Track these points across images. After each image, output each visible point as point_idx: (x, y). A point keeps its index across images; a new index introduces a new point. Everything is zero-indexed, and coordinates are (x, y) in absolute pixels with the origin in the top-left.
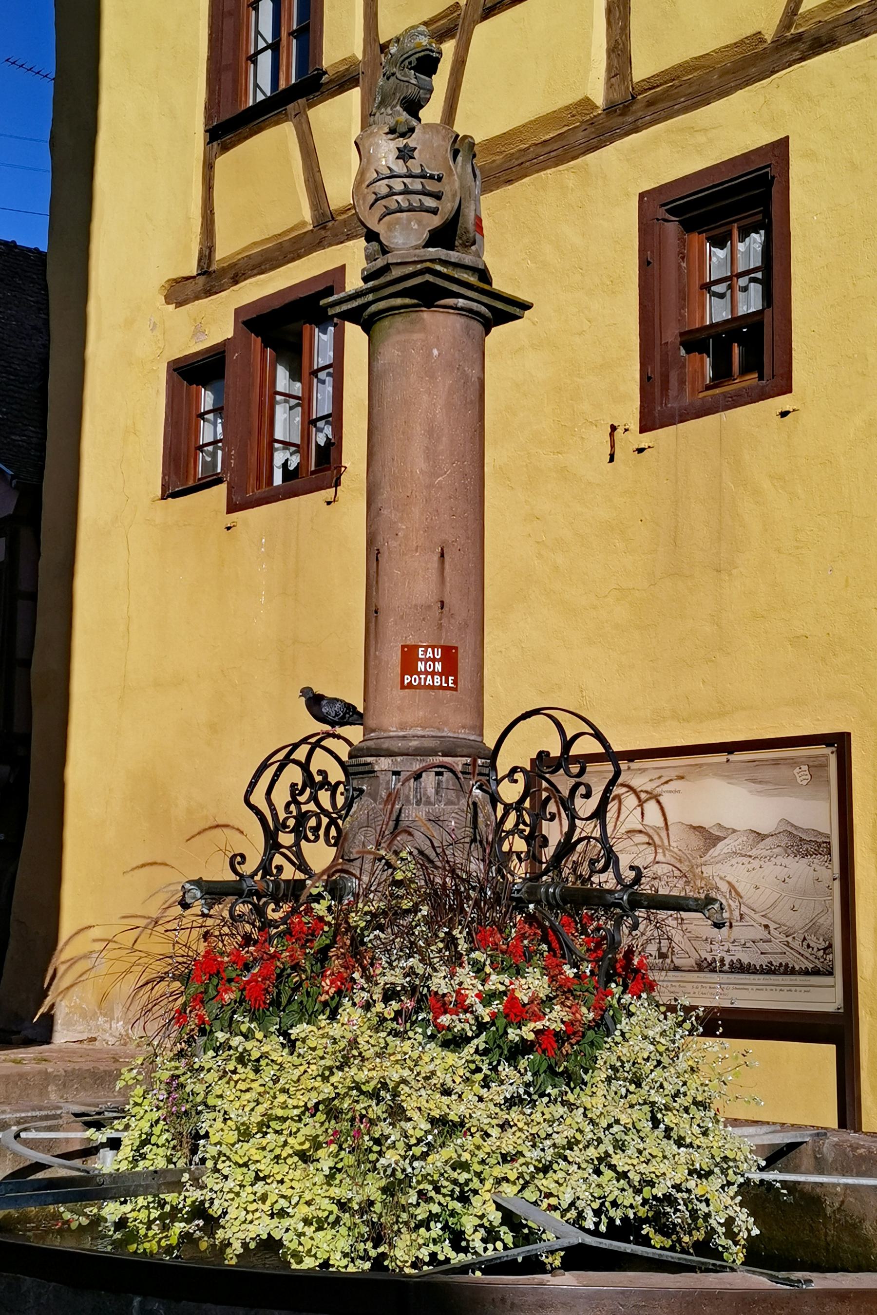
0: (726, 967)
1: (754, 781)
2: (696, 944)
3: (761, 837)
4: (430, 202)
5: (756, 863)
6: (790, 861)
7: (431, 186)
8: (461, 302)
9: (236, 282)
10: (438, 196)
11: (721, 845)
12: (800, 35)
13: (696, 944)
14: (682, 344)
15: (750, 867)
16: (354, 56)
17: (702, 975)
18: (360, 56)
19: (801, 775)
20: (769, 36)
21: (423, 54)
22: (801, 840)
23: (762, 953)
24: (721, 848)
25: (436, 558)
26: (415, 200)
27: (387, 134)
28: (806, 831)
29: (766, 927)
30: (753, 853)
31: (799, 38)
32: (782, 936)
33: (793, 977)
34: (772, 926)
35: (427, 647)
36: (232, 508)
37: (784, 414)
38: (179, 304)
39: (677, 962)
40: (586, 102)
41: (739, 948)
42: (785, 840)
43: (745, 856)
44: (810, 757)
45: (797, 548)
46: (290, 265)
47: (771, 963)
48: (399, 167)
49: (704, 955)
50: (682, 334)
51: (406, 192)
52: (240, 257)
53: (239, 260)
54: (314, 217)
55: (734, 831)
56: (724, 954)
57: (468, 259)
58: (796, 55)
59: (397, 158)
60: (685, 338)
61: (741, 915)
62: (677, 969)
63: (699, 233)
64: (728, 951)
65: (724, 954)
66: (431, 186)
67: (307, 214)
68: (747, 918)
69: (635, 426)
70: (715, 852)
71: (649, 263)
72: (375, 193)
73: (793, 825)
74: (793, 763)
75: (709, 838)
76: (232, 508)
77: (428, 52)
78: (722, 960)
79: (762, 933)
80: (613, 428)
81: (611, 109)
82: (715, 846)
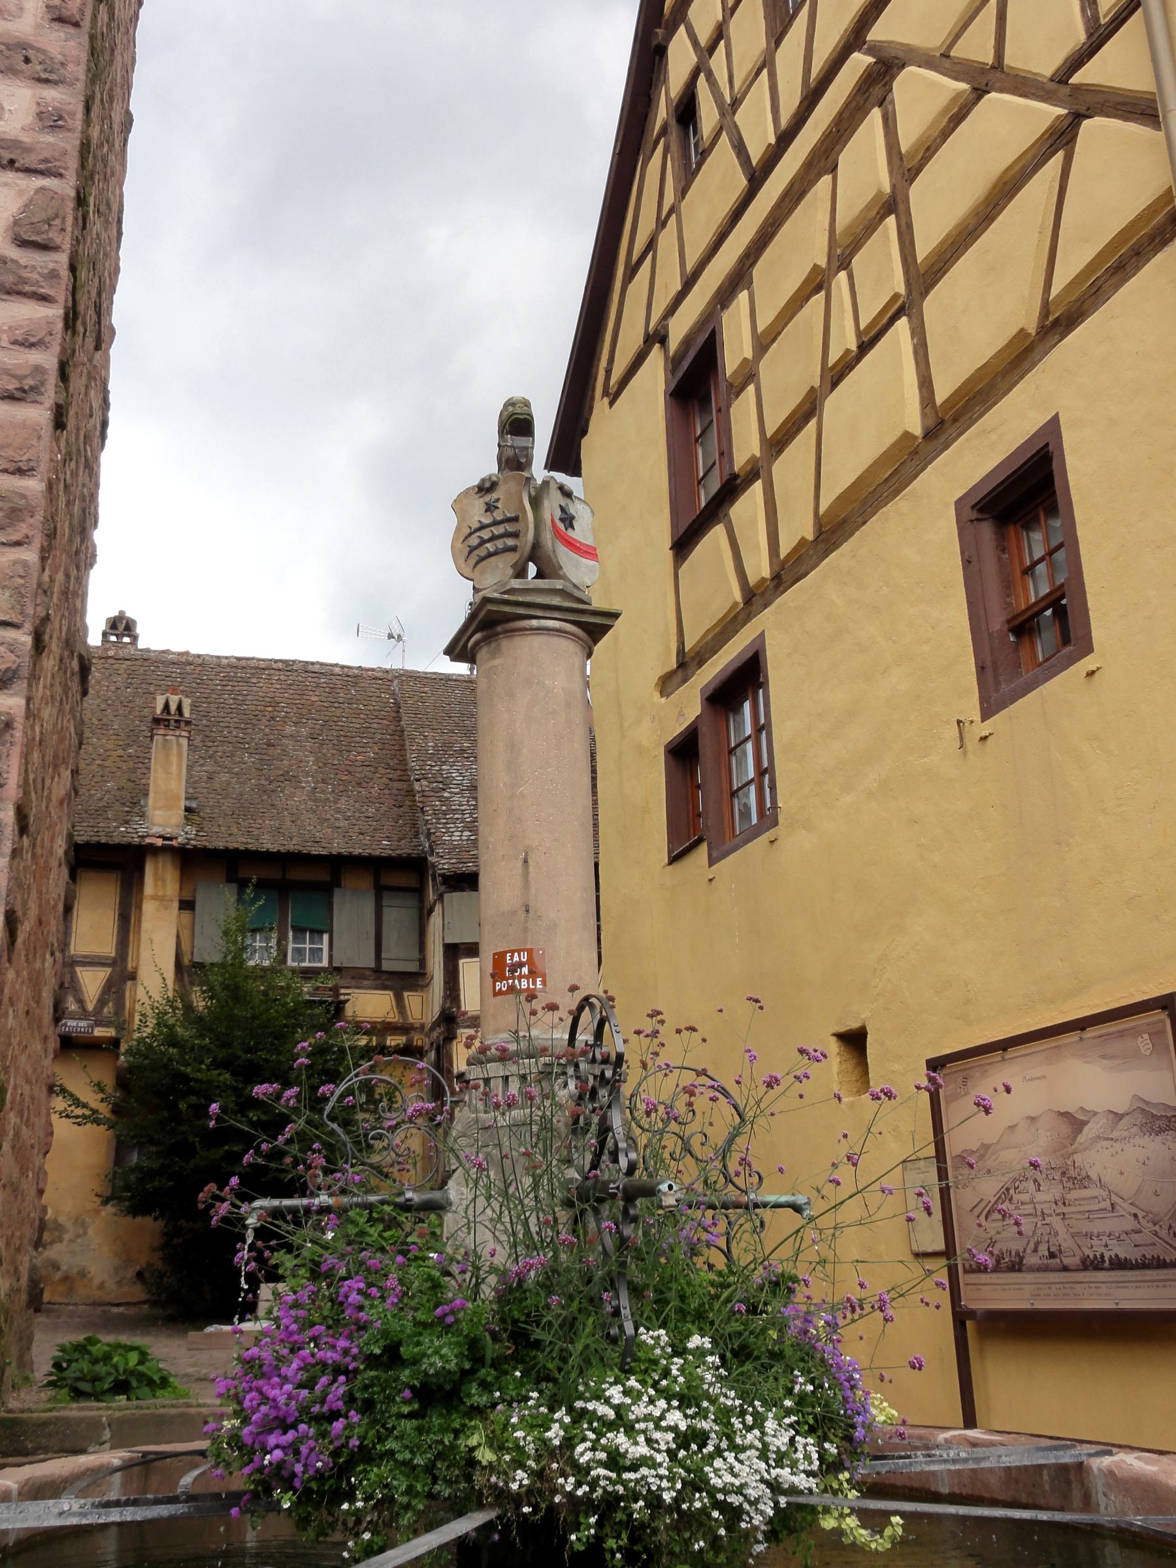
0: (1107, 1264)
1: (1104, 1057)
2: (1079, 1240)
3: (1119, 1117)
4: (510, 542)
5: (1118, 1146)
6: (1146, 1140)
7: (510, 528)
8: (534, 623)
9: (700, 667)
10: (515, 535)
11: (1086, 1129)
12: (1057, 319)
13: (1079, 1240)
14: (1010, 630)
15: (1113, 1150)
16: (754, 456)
17: (1087, 1274)
18: (758, 454)
19: (1144, 1044)
20: (1032, 330)
22: (1153, 1116)
23: (1136, 1246)
24: (1088, 1133)
25: (520, 864)
26: (500, 544)
28: (1156, 1105)
29: (1135, 1216)
30: (1114, 1135)
31: (1056, 322)
32: (1150, 1225)
33: (1166, 1271)
34: (1140, 1214)
35: (513, 952)
36: (712, 862)
37: (1091, 674)
38: (668, 696)
39: (1066, 1261)
40: (907, 436)
41: (1115, 1242)
42: (1139, 1118)
43: (1107, 1139)
44: (1149, 1024)
45: (1119, 806)
47: (1144, 1256)
48: (486, 520)
49: (1087, 1252)
50: (1008, 621)
51: (493, 538)
54: (743, 597)
55: (1095, 1113)
56: (1103, 1250)
57: (558, 584)
58: (1057, 337)
60: (1012, 624)
61: (1112, 1205)
62: (1065, 1269)
63: (1015, 523)
64: (1106, 1246)
65: (1103, 1250)
66: (510, 528)
67: (738, 596)
68: (1118, 1207)
69: (976, 716)
70: (1081, 1138)
71: (969, 562)
73: (1144, 1101)
74: (1135, 1033)
75: (1074, 1123)
76: (712, 862)
78: (1102, 1256)
79: (1130, 1224)
80: (959, 722)
81: (929, 435)
82: (1081, 1131)
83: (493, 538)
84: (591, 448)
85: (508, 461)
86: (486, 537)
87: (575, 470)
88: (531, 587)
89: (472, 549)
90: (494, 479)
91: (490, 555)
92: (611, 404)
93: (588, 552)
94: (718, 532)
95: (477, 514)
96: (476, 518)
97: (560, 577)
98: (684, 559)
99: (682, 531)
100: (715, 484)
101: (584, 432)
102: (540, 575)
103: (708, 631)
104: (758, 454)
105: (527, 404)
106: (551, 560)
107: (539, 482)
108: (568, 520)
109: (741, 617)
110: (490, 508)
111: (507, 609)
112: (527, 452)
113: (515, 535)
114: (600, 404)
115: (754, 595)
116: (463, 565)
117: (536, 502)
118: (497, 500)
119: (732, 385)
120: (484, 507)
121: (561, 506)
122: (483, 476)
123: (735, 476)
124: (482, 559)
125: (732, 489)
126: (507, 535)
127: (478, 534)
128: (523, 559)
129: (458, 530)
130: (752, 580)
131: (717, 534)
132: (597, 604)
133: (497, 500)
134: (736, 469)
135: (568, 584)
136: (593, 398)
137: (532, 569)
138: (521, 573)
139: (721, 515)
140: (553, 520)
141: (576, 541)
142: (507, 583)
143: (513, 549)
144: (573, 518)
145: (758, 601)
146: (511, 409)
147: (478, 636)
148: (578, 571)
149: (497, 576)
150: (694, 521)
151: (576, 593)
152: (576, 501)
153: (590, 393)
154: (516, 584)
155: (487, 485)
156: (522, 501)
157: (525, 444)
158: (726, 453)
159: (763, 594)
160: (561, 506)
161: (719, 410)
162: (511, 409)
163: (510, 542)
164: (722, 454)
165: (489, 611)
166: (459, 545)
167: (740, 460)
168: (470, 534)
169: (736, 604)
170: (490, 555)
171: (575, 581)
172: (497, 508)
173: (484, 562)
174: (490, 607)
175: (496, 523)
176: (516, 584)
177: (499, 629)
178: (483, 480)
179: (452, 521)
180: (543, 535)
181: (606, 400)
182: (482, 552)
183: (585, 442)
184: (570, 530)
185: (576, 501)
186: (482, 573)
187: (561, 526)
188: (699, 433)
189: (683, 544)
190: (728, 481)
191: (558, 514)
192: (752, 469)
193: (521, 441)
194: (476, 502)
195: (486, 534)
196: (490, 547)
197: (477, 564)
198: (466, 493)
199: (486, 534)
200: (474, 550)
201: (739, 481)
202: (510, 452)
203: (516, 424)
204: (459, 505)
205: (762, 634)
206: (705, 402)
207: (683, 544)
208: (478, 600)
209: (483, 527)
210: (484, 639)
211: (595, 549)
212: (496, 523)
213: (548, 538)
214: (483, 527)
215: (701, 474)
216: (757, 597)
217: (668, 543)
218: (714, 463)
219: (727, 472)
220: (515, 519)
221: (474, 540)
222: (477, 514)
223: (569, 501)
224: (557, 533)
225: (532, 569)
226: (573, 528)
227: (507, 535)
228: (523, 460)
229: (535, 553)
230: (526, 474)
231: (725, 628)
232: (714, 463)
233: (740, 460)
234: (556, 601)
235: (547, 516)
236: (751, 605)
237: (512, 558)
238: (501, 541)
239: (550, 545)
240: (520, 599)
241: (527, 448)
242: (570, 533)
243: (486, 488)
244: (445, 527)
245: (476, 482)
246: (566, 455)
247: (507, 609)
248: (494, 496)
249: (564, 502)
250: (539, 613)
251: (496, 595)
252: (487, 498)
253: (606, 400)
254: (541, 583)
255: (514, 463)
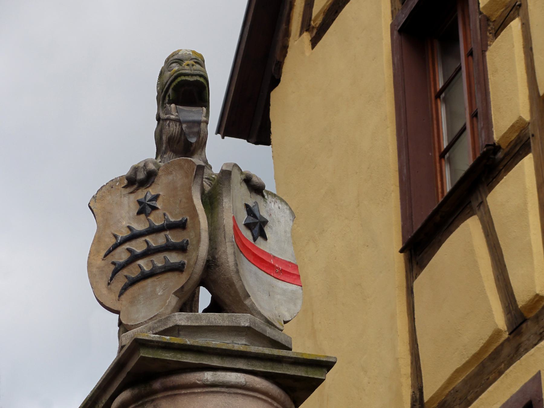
4: (174, 258)
7: (174, 237)
8: (208, 376)
10: (182, 248)
16: (521, 119)
18: (527, 117)
21: (174, 84)
26: (159, 260)
27: (125, 187)
46: (490, 388)
48: (139, 226)
51: (149, 252)
52: (447, 391)
53: (447, 395)
54: (509, 322)
57: (244, 320)
59: (139, 213)
66: (174, 237)
67: (500, 321)
72: (113, 263)
77: (198, 78)
83: (149, 252)
84: (286, 104)
85: (171, 140)
86: (138, 251)
87: (260, 134)
88: (204, 323)
89: (118, 268)
90: (151, 167)
91: (145, 276)
92: (314, 42)
93: (287, 272)
94: (470, 229)
95: (126, 217)
96: (125, 223)
97: (245, 309)
98: (422, 266)
99: (418, 226)
100: (465, 159)
101: (275, 82)
102: (215, 307)
103: (458, 372)
104: (527, 117)
105: (199, 61)
106: (232, 285)
107: (216, 170)
108: (258, 226)
109: (506, 351)
110: (145, 209)
111: (168, 356)
112: (198, 127)
113: (182, 248)
114: (298, 43)
115: (525, 320)
116: (104, 291)
117: (211, 201)
118: (156, 198)
119: (488, 19)
120: (135, 208)
121: (247, 206)
122: (135, 163)
123: (494, 148)
124: (133, 282)
125: (491, 165)
126: (168, 248)
127: (127, 246)
128: (192, 282)
129: (98, 240)
130: (522, 297)
131: (469, 232)
132: (301, 347)
133: (156, 198)
134: (496, 137)
135: (258, 320)
136: (287, 34)
137: (205, 298)
138: (188, 304)
139: (475, 204)
140: (235, 227)
141: (269, 255)
142: (167, 319)
143: (179, 268)
144: (265, 222)
145: (530, 329)
146: (176, 67)
147: (125, 395)
148: (271, 299)
149: (154, 306)
150: (435, 212)
151: (270, 332)
152: (269, 199)
153: (284, 26)
154: (182, 319)
155: (141, 176)
156: (190, 199)
157: (196, 118)
158: (481, 114)
159: (537, 317)
160: (247, 206)
161: (470, 54)
162: (176, 67)
163: (174, 258)
164: (474, 115)
165: (143, 358)
166: (99, 261)
167: (501, 125)
168: (115, 247)
169: (498, 333)
170: (145, 276)
171: (267, 314)
172: (154, 208)
173: (136, 288)
174: (144, 353)
175: (153, 231)
176: (182, 319)
177: (157, 385)
178: (135, 169)
179: (89, 227)
180: (222, 249)
181: (307, 37)
182: (133, 272)
183: (275, 95)
184: (260, 239)
185: (269, 199)
186: (133, 302)
187: (247, 234)
188: (440, 84)
189: (420, 245)
190: (484, 155)
191: (243, 217)
192: (519, 137)
193: (191, 113)
194: (125, 200)
195: (138, 246)
196: (144, 264)
197: (125, 289)
198: (111, 186)
199: (138, 246)
200: (120, 269)
201: (500, 155)
202: (174, 129)
203: (182, 88)
204: (99, 205)
205: (538, 377)
206: (449, 42)
207: (420, 245)
208: (127, 342)
209: (134, 236)
210: (134, 399)
211: (295, 267)
212: (153, 231)
213: (228, 253)
214: (134, 236)
215: (445, 144)
216: (529, 323)
217: (397, 243)
218: (464, 129)
219: (482, 140)
220: (181, 226)
221: (121, 255)
222: (126, 217)
223: (259, 198)
224: (243, 247)
225: (205, 298)
226: (265, 238)
227: (168, 248)
228: (193, 140)
229: (211, 274)
230: (196, 160)
231: (483, 366)
232: (464, 129)
233: (501, 125)
234: (239, 344)
235: (227, 221)
236: (520, 334)
237: (175, 281)
238: (161, 256)
239: (231, 260)
240: (189, 341)
241: (199, 123)
242: (260, 244)
243: (139, 180)
244: (82, 234)
245: (125, 171)
246: (249, 118)
247: (168, 356)
248: (152, 191)
249: (251, 200)
250: (216, 362)
251: (152, 336)
252: (141, 194)
253: (307, 37)
254: (217, 319)
255: (179, 143)
